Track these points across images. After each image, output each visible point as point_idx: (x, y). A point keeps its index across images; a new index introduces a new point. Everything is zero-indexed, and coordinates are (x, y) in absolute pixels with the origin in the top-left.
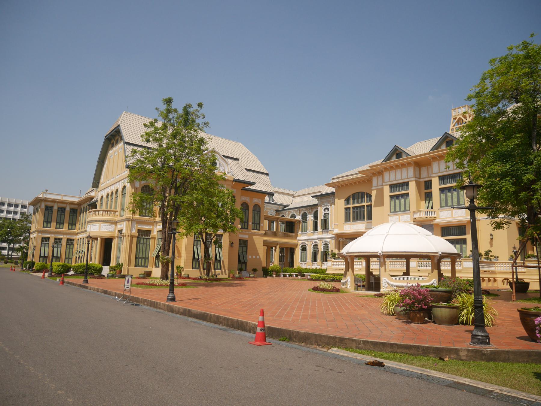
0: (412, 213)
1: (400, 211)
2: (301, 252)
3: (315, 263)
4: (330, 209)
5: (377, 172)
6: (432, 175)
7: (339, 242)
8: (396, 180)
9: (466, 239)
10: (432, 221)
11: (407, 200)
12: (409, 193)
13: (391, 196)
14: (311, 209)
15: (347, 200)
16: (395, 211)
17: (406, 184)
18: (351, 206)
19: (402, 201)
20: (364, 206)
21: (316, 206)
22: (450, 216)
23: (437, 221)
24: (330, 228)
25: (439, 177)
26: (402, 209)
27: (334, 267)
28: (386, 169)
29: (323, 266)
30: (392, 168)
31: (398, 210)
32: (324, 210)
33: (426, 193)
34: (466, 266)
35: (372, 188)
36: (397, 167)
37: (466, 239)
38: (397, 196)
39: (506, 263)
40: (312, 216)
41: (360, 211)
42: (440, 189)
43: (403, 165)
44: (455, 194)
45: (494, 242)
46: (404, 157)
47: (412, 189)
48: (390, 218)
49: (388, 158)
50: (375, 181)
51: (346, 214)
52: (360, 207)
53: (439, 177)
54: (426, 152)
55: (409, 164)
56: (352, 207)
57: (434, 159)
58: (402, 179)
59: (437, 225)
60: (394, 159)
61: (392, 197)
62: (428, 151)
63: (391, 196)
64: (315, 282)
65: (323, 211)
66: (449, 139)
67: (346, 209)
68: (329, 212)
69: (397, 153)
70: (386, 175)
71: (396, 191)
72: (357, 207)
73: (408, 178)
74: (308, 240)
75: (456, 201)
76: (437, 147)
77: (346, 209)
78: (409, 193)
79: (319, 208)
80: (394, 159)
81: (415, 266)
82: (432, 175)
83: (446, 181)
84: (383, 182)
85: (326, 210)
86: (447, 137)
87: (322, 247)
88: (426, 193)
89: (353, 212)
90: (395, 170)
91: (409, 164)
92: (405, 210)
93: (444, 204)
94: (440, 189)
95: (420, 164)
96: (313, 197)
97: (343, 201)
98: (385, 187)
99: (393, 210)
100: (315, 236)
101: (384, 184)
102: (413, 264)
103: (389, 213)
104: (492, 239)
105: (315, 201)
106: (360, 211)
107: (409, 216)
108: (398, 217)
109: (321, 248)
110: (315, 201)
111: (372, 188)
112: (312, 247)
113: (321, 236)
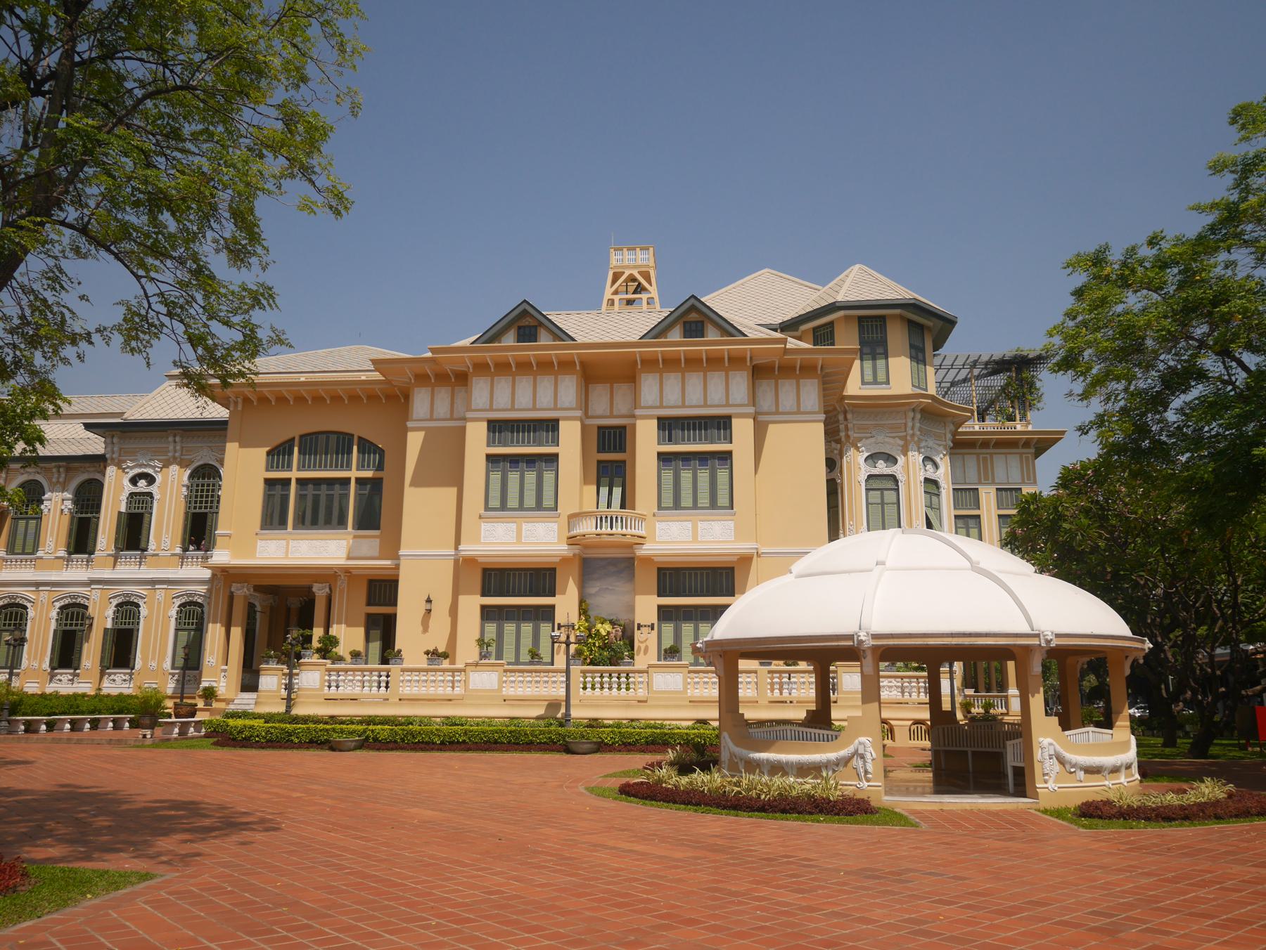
0: (564, 519)
1: (521, 507)
2: (177, 630)
3: (65, 675)
4: (159, 478)
5: (452, 376)
6: (469, 415)
7: (231, 597)
8: (705, 405)
9: (553, 607)
10: (630, 546)
11: (548, 477)
12: (730, 453)
13: (491, 458)
14: (68, 470)
15: (279, 454)
16: (503, 506)
17: (551, 426)
18: (294, 474)
19: (531, 477)
20: (346, 481)
21: (99, 461)
22: (512, 537)
23: (647, 549)
24: (152, 546)
25: (660, 419)
26: (530, 500)
27: (509, 691)
28: (481, 368)
29: (106, 683)
30: (503, 368)
31: (513, 501)
32: (134, 481)
33: (599, 462)
34: (663, 688)
35: (409, 424)
36: (524, 367)
37: (553, 607)
38: (514, 460)
39: (419, 670)
40: (68, 495)
41: (330, 498)
42: (659, 454)
43: (545, 366)
44: (704, 476)
45: (432, 623)
46: (544, 339)
47: (570, 444)
48: (485, 526)
49: (493, 336)
50: (421, 402)
51: (268, 498)
52: (330, 482)
53: (660, 419)
54: (629, 339)
55: (565, 366)
56: (299, 481)
57: (481, 368)
58: (513, 409)
59: (648, 560)
60: (509, 340)
61: (664, 458)
62: (635, 337)
63: (491, 458)
64: (618, 757)
65: (126, 482)
66: (526, 322)
67: (269, 483)
68: (154, 489)
69: (526, 323)
70: (480, 390)
71: (511, 444)
72: (317, 482)
73: (555, 408)
74: (37, 584)
75: (707, 495)
76: (659, 331)
77: (269, 483)
78: (730, 453)
79: (111, 471)
80: (509, 340)
81: (317, 685)
82: (469, 415)
83: (677, 433)
84: (636, 403)
85: (142, 483)
86: (693, 308)
87: (110, 612)
88: (599, 462)
89: (301, 498)
90: (514, 375)
91: (565, 366)
92: (539, 506)
93: (668, 500)
94: (659, 454)
95: (604, 371)
96: (88, 427)
97: (260, 454)
98: (470, 427)
99: (495, 503)
100: (77, 572)
101: (638, 412)
102: (849, 679)
103: (482, 511)
104: (429, 611)
105: (96, 445)
106: (330, 498)
107: (554, 526)
108: (514, 526)
109: (103, 616)
110: (96, 445)
111: (409, 424)
112: (54, 614)
113: (107, 574)
